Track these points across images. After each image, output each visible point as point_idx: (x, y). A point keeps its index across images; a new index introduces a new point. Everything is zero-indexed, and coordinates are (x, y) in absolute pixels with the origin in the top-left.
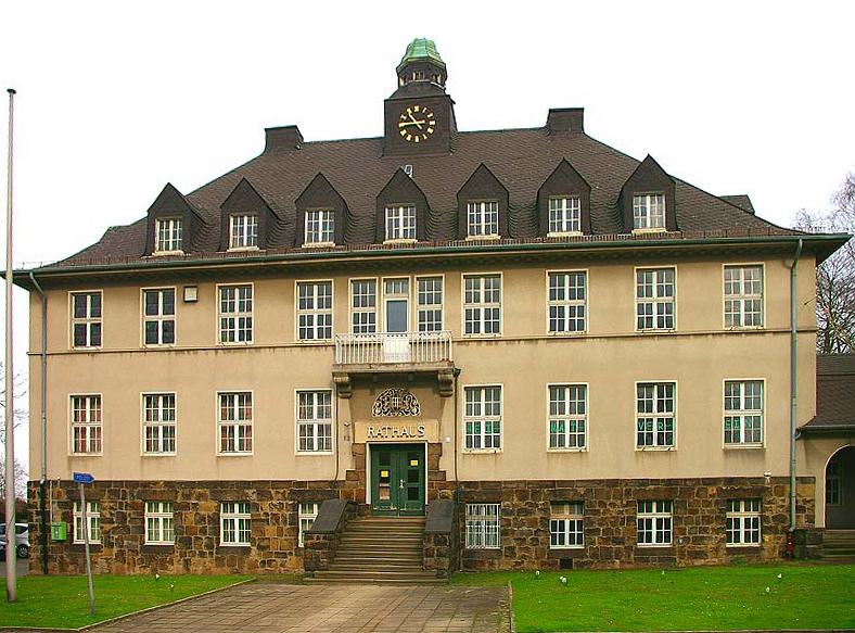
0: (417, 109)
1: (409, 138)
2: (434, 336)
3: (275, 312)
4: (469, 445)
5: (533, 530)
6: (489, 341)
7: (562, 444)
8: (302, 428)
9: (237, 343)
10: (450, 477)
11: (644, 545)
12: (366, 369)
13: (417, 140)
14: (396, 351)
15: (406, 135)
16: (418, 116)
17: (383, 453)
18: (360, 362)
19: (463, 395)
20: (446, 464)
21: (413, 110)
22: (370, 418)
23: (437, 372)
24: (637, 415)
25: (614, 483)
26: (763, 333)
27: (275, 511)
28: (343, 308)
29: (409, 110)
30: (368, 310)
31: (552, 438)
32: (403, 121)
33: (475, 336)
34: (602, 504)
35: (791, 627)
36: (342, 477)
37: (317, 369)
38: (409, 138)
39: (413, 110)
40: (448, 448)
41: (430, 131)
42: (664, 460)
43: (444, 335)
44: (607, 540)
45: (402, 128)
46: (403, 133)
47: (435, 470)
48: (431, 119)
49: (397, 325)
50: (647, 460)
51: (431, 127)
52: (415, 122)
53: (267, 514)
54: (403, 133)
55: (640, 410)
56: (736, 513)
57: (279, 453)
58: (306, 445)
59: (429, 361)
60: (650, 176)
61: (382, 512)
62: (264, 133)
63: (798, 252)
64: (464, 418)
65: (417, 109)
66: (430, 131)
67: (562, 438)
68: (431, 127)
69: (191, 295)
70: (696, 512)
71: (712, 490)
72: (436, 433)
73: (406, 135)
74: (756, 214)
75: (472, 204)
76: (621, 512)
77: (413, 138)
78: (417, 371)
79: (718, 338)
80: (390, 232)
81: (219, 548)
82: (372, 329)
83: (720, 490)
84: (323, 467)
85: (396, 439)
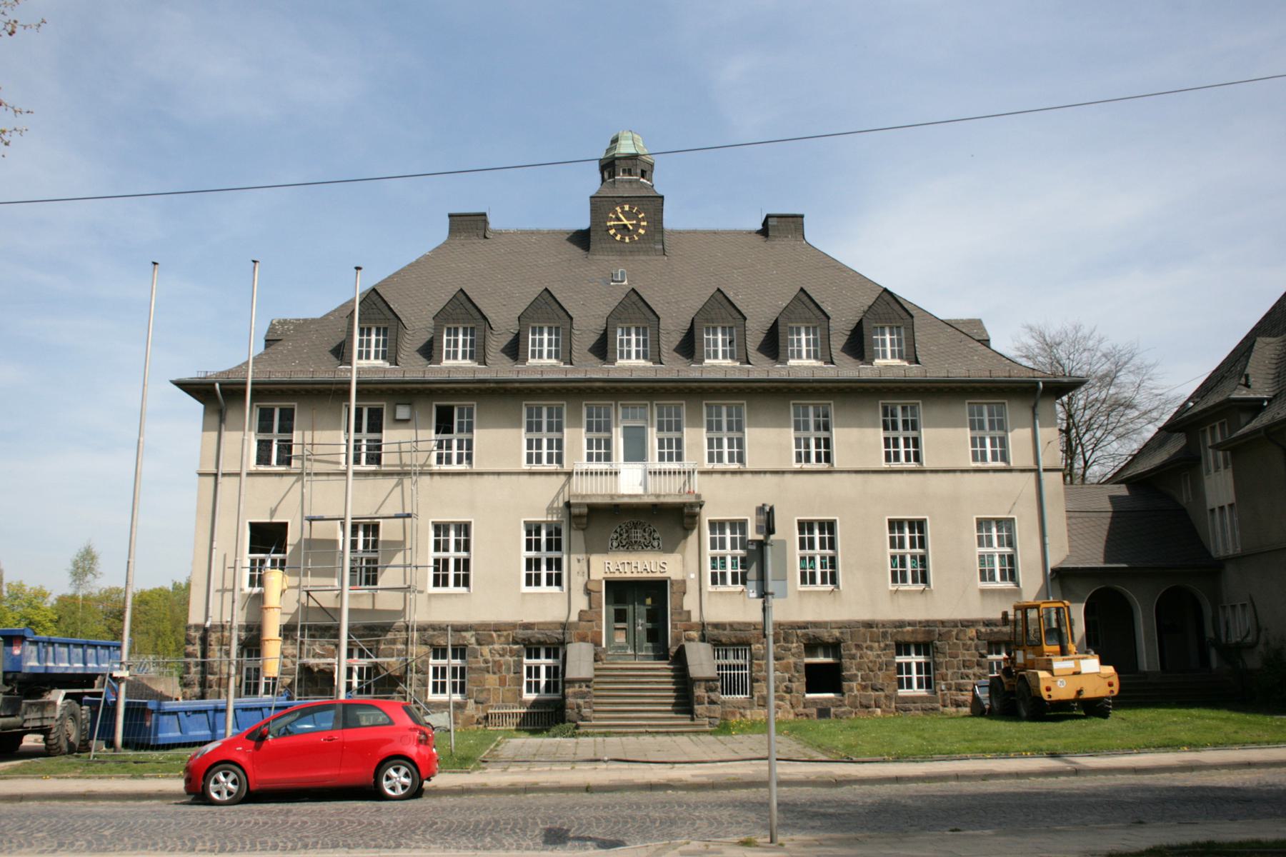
0: (627, 208)
1: (618, 238)
2: (674, 466)
3: (501, 443)
4: (714, 582)
5: (787, 675)
6: (734, 473)
7: (813, 581)
8: (529, 561)
9: (455, 467)
10: (695, 618)
11: (903, 692)
12: (607, 500)
13: (627, 240)
14: (630, 482)
15: (615, 235)
16: (629, 215)
17: (619, 591)
18: (591, 489)
19: (707, 535)
20: (690, 603)
21: (622, 208)
22: (605, 550)
23: (684, 504)
24: (890, 551)
25: (869, 625)
26: (1010, 471)
27: (497, 658)
28: (576, 439)
29: (618, 209)
30: (603, 435)
31: (803, 575)
32: (611, 219)
33: (718, 466)
34: (858, 647)
35: (1192, 716)
36: (574, 617)
37: (540, 499)
38: (618, 238)
39: (622, 208)
40: (692, 588)
41: (642, 231)
42: (920, 600)
43: (687, 464)
44: (864, 688)
45: (611, 227)
46: (612, 232)
47: (680, 610)
48: (643, 219)
49: (636, 452)
50: (902, 600)
51: (643, 227)
52: (626, 222)
53: (486, 662)
54: (612, 232)
55: (893, 546)
56: (811, 552)
57: (504, 593)
58: (533, 580)
59: (668, 490)
60: (891, 309)
61: (619, 657)
62: (447, 220)
63: (1039, 393)
64: (708, 552)
65: (627, 208)
66: (642, 231)
67: (813, 575)
68: (643, 227)
69: (403, 412)
70: (956, 656)
71: (972, 632)
72: (679, 567)
73: (615, 235)
74: (993, 345)
75: (708, 329)
76: (879, 656)
77: (623, 239)
78: (662, 504)
79: (966, 475)
80: (622, 352)
81: (427, 704)
82: (608, 458)
83: (978, 633)
84: (548, 606)
85: (635, 575)
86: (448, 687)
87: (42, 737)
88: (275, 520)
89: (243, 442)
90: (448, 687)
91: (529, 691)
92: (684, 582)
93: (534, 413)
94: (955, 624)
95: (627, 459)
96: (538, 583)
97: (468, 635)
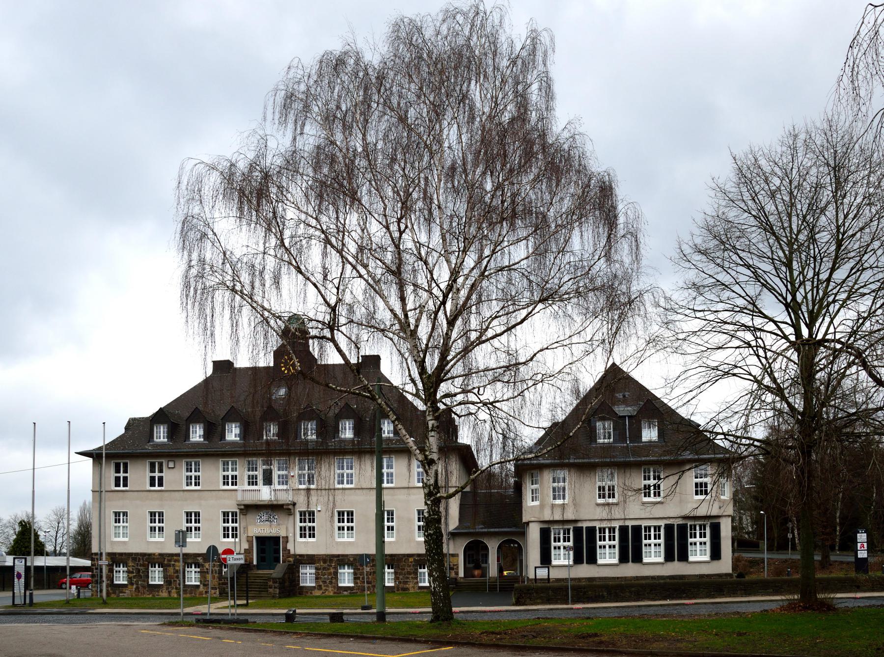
2: (285, 487)
10: (292, 552)
18: (250, 499)
20: (290, 546)
40: (291, 539)
47: (285, 549)
49: (268, 481)
59: (285, 498)
69: (171, 465)
71: (411, 559)
86: (652, 477)
87: (116, 582)
88: (692, 419)
89: (110, 474)
90: (652, 477)
91: (600, 497)
92: (287, 537)
93: (225, 464)
94: (404, 555)
95: (264, 484)
96: (228, 537)
97: (199, 558)
